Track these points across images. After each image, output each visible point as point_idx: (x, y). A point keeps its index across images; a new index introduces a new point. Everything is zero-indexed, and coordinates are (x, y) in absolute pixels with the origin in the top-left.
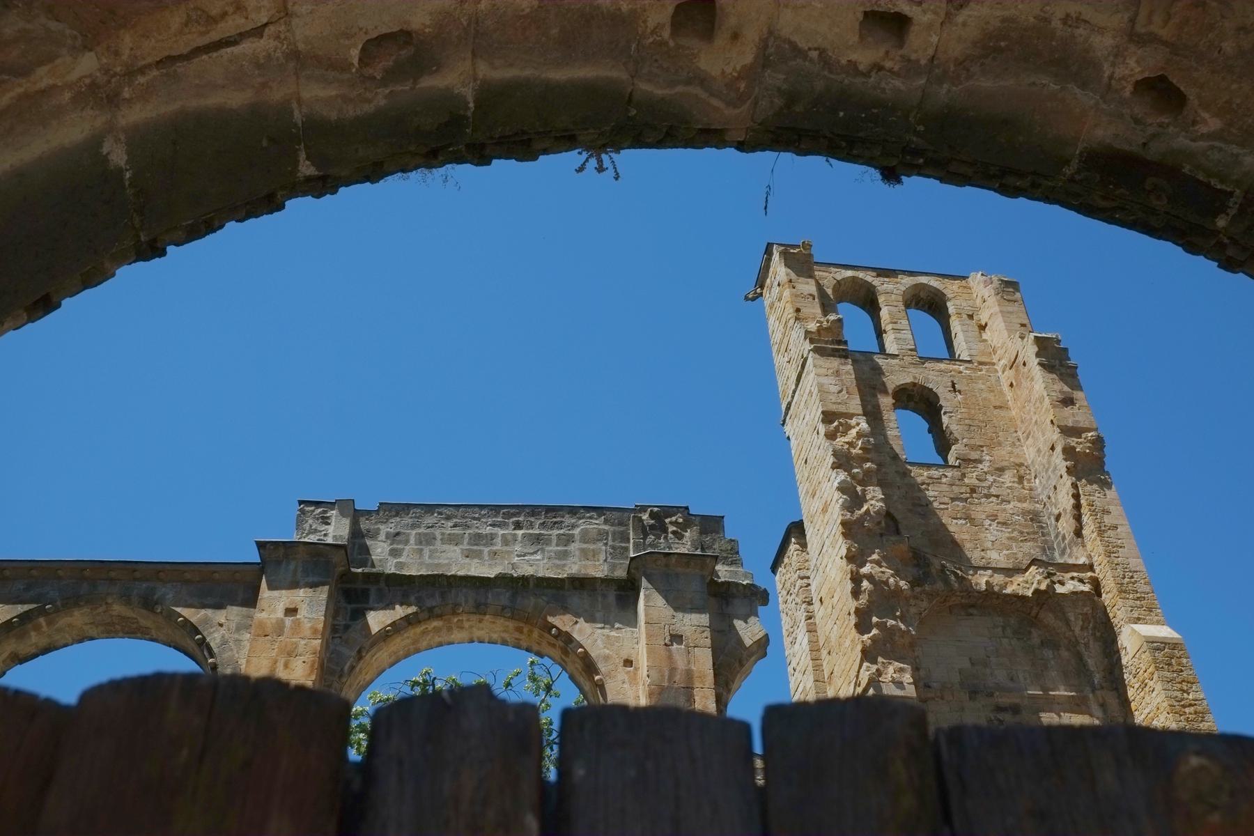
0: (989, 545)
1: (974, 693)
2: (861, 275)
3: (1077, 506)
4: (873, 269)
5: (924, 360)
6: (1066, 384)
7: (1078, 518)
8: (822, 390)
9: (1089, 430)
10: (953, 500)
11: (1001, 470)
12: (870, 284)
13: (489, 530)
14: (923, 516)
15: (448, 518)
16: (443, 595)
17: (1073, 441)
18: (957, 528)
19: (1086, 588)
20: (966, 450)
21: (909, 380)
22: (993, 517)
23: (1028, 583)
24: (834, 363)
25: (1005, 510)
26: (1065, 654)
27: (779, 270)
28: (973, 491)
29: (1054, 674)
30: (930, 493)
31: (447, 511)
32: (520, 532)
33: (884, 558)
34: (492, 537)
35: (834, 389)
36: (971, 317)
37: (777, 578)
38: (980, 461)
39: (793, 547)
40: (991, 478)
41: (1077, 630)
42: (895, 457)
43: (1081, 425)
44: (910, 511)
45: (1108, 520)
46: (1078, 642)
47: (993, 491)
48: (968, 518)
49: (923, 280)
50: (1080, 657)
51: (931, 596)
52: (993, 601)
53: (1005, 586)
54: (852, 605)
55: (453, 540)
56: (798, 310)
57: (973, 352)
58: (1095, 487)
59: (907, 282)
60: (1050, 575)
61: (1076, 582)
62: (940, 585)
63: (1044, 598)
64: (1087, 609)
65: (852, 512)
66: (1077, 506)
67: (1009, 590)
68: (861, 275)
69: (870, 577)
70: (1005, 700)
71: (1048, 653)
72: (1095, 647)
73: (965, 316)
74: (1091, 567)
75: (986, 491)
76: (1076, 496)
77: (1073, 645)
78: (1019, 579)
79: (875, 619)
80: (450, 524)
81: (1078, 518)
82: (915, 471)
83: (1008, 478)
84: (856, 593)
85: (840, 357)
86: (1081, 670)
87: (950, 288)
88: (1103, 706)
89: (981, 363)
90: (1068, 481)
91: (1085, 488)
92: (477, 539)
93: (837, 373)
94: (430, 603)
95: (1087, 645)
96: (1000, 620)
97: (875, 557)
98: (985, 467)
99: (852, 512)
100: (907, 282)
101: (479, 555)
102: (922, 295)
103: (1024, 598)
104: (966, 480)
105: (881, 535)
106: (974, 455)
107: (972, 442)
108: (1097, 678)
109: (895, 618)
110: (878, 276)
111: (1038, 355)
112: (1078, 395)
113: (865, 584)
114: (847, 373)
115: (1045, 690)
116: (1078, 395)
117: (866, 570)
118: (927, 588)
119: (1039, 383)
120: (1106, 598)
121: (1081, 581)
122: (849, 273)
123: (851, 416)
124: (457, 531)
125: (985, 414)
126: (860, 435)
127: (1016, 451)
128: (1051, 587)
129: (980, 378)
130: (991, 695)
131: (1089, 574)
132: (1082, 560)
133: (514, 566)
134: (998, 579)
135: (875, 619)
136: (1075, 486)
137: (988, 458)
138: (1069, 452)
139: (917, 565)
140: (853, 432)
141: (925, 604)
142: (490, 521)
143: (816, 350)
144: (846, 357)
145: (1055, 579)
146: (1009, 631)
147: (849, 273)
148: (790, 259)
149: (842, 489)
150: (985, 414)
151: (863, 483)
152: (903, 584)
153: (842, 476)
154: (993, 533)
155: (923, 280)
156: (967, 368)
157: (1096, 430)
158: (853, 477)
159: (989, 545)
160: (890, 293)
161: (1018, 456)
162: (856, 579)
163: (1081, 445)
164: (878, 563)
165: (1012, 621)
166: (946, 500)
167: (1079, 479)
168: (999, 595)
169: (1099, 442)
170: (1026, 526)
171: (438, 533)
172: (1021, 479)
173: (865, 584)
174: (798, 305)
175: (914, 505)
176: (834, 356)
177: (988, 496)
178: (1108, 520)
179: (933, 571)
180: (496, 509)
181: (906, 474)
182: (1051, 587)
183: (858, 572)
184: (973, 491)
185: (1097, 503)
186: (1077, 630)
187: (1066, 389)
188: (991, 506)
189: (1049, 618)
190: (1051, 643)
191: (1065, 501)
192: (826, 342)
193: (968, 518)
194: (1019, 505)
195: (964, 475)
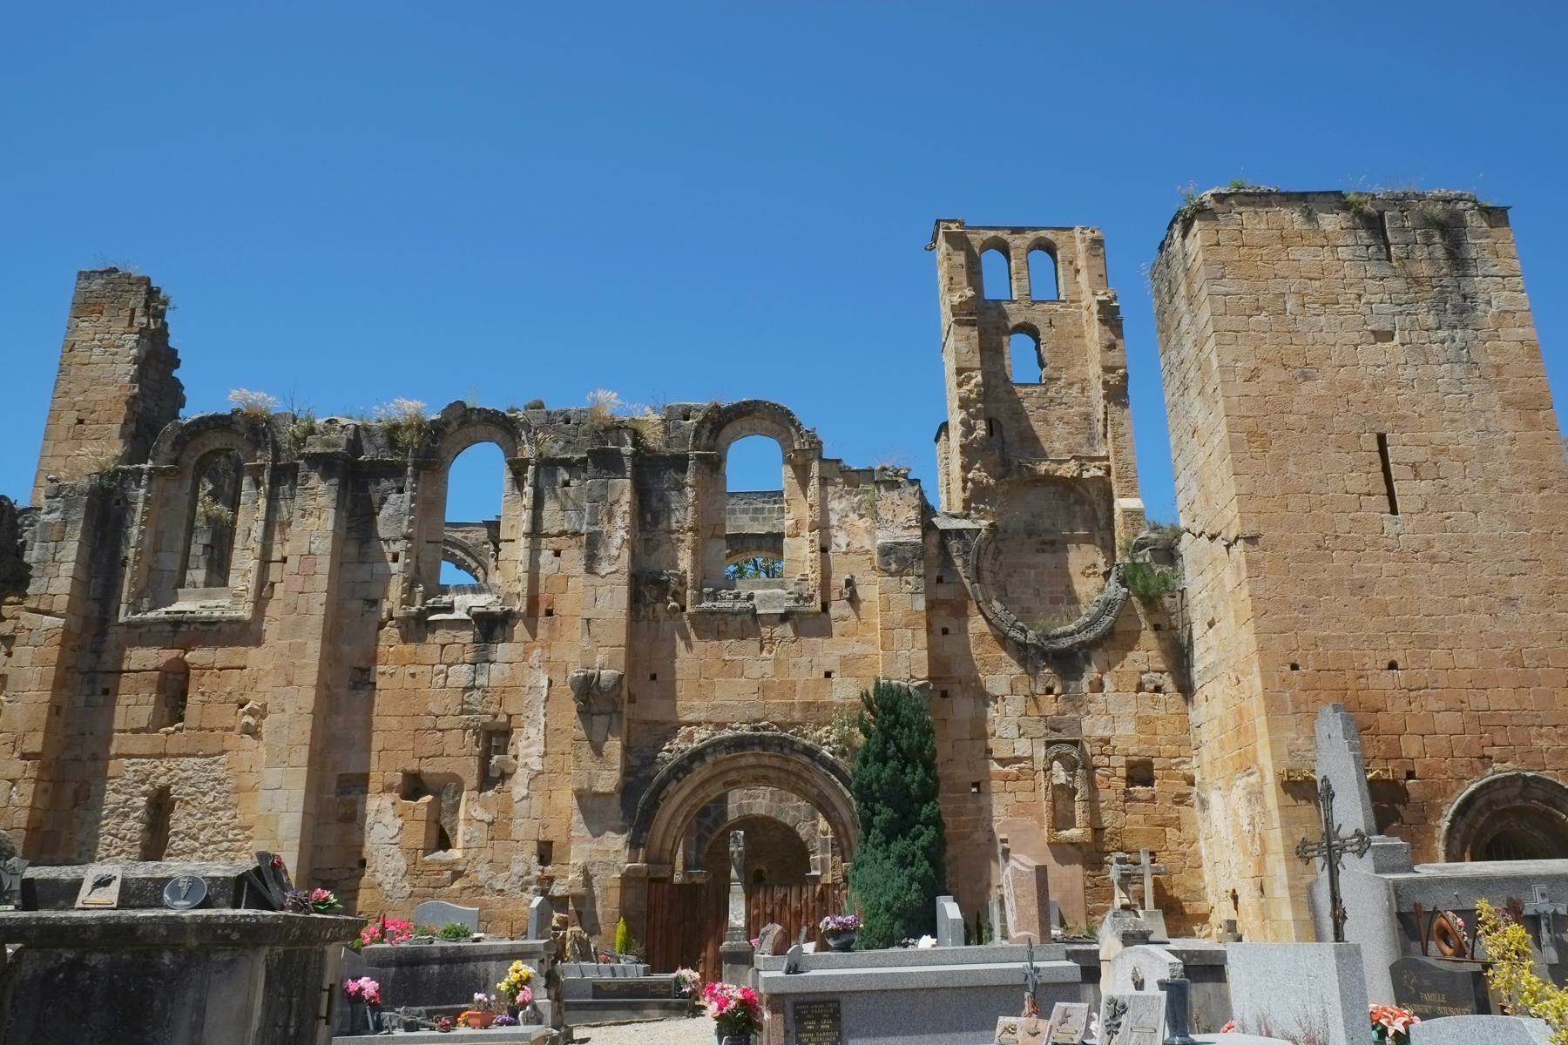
0: (1055, 438)
1: (1030, 534)
2: (1000, 234)
3: (1106, 419)
4: (1009, 228)
5: (1034, 302)
6: (1113, 333)
7: (1105, 426)
8: (957, 351)
9: (1120, 368)
10: (1038, 408)
11: (1072, 384)
12: (790, 833)
13: (761, 505)
14: (1018, 421)
15: (742, 500)
16: (742, 543)
17: (1108, 377)
18: (1038, 427)
19: (1100, 473)
20: (1052, 372)
21: (1021, 320)
22: (1061, 419)
23: (1069, 470)
24: (967, 330)
25: (1069, 413)
26: (1087, 508)
27: (942, 245)
28: (1051, 401)
29: (1078, 520)
30: (1025, 405)
31: (740, 496)
32: (777, 506)
33: (983, 465)
34: (763, 509)
35: (964, 350)
36: (1071, 263)
37: (938, 447)
38: (1059, 379)
39: (943, 437)
40: (1063, 391)
41: (1094, 497)
42: (1007, 380)
43: (1117, 364)
44: (1010, 418)
45: (1121, 430)
46: (1093, 503)
47: (1064, 401)
48: (1046, 421)
49: (1042, 233)
50: (1094, 510)
51: (1010, 483)
52: (1049, 480)
53: (1056, 471)
54: (962, 495)
55: (745, 511)
56: (951, 279)
57: (1068, 293)
58: (1119, 407)
59: (1031, 236)
60: (1082, 465)
61: (1095, 469)
62: (1016, 477)
63: (1077, 480)
64: (1101, 485)
65: (967, 438)
66: (1106, 419)
67: (1058, 474)
68: (1000, 234)
69: (973, 480)
70: (1048, 537)
71: (1077, 508)
72: (1103, 505)
73: (1067, 263)
74: (1107, 458)
75: (1059, 401)
76: (1106, 413)
77: (1091, 504)
78: (1065, 466)
79: (973, 505)
80: (743, 502)
81: (1105, 426)
82: (1017, 389)
83: (1075, 390)
84: (964, 489)
85: (971, 325)
86: (1095, 519)
87: (1060, 239)
88: (1102, 539)
89: (1072, 302)
90: (1102, 402)
91: (1112, 408)
92: (756, 510)
93: (968, 338)
94: (736, 547)
95: (1098, 505)
96: (1052, 489)
97: (978, 466)
98: (1061, 383)
99: (967, 438)
100: (1031, 236)
101: (756, 519)
102: (1042, 243)
103: (1066, 478)
104: (1049, 394)
105: (983, 450)
106: (1056, 375)
107: (1056, 365)
108: (1102, 523)
109: (984, 503)
110: (1012, 233)
111: (1099, 312)
112: (1119, 342)
113: (969, 484)
114: (975, 337)
115: (1072, 531)
116: (1119, 342)
117: (970, 476)
118: (1007, 479)
119: (1094, 333)
120: (1113, 478)
121: (1100, 468)
122: (992, 233)
123: (972, 370)
124: (746, 506)
125: (1067, 343)
126: (976, 385)
127: (1084, 369)
128: (1080, 474)
129: (1069, 314)
130: (1040, 535)
131: (1105, 463)
132: (1103, 454)
133: (774, 525)
134: (1054, 466)
135: (973, 505)
136: (1105, 407)
137: (1064, 376)
138: (1106, 384)
139: (1003, 465)
140: (973, 381)
141: (1006, 487)
142: (762, 500)
143: (956, 322)
144: (974, 325)
145: (1084, 468)
146: (1057, 495)
147: (992, 233)
148: (950, 237)
149: (963, 422)
150: (1067, 343)
151: (975, 417)
152: (992, 481)
153: (963, 414)
154: (1060, 429)
155: (1042, 233)
156: (1062, 307)
157: (1125, 368)
158: (969, 414)
159: (1055, 438)
160: (1018, 243)
161: (1084, 373)
162: (965, 481)
163: (1113, 379)
164: (979, 470)
165: (1060, 489)
166: (1034, 409)
167: (1109, 402)
168: (1053, 476)
169: (1125, 377)
170: (1079, 424)
171: (737, 507)
172: (1083, 389)
173: (969, 484)
174: (952, 275)
175: (1013, 414)
176: (966, 325)
177: (1060, 404)
178: (1121, 430)
179: (1013, 467)
180: (764, 494)
181: (1013, 392)
182: (1080, 474)
183: (966, 477)
184: (1051, 401)
185: (1116, 419)
186: (1094, 497)
187: (1113, 337)
188: (1059, 411)
189: (1079, 488)
190: (1081, 501)
191: (1101, 409)
192: (963, 315)
193: (1046, 421)
194: (1078, 409)
195: (1047, 390)
